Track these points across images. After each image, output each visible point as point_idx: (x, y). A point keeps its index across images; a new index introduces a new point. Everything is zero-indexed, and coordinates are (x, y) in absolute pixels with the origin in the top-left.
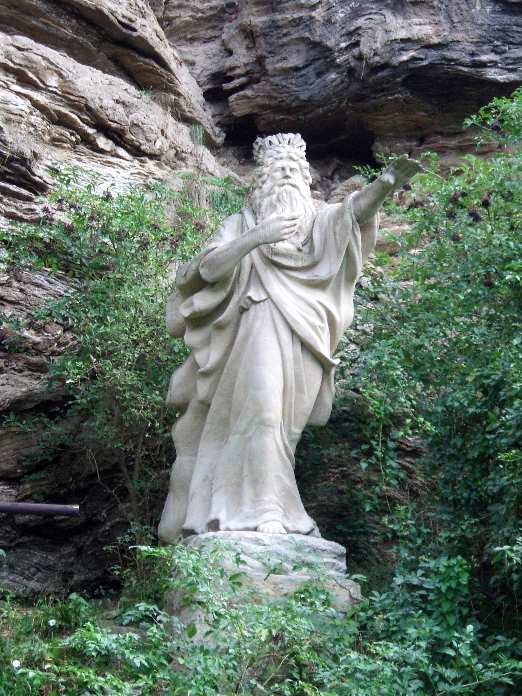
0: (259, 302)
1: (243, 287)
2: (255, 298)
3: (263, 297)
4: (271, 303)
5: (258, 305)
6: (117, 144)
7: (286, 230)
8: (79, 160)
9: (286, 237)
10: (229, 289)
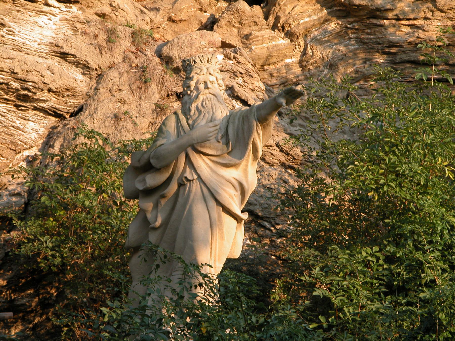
2: (190, 178)
8: (19, 11)
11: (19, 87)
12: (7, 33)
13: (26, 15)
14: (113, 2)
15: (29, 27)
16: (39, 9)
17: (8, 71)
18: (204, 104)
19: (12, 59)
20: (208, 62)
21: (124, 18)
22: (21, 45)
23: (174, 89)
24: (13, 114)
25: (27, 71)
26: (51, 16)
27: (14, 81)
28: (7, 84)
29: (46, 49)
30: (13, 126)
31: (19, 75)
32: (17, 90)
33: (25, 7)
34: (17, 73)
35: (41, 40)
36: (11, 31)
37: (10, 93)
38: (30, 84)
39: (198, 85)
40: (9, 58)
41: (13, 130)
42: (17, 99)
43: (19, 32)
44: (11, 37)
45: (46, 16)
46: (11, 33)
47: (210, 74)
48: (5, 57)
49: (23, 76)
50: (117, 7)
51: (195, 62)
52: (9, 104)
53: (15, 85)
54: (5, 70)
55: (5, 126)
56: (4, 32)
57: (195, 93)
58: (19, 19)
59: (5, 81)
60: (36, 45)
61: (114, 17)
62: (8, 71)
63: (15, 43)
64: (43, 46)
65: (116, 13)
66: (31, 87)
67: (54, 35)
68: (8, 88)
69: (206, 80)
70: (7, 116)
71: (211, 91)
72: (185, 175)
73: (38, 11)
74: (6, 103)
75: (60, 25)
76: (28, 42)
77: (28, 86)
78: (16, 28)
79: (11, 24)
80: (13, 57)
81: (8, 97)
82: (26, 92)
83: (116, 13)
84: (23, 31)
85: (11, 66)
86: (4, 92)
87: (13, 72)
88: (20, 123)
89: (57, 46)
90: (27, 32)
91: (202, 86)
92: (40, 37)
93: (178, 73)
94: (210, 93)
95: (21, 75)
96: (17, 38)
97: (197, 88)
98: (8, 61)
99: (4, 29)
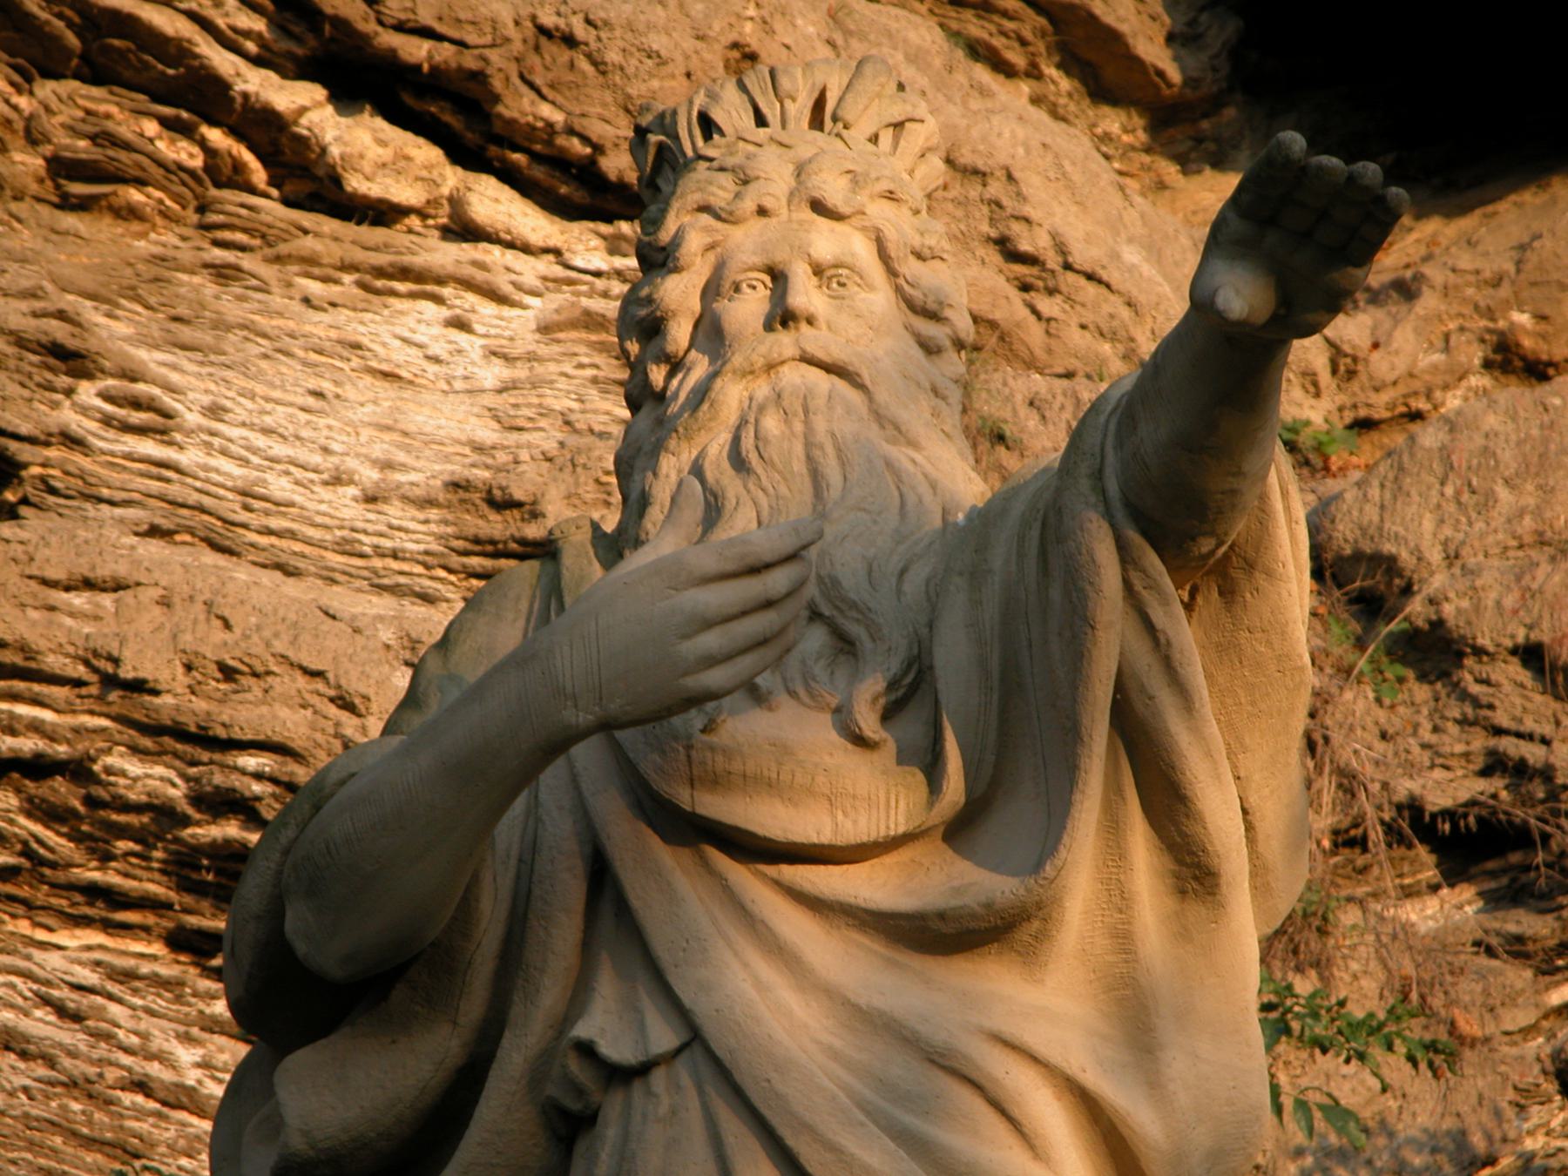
0: (643, 1070)
1: (550, 995)
2: (618, 1049)
3: (663, 1037)
4: (706, 1071)
5: (637, 1086)
6: (465, 156)
7: (711, 641)
8: (223, 274)
9: (715, 678)
10: (473, 1006)
11: (177, 793)
12: (107, 421)
13: (277, 300)
14: (1017, 228)
15: (294, 378)
16: (381, 259)
17: (81, 671)
18: (748, 442)
19: (118, 586)
20: (817, 121)
21: (1110, 336)
22: (231, 506)
23: (1405, 787)
24: (160, 1004)
25: (228, 673)
26: (471, 298)
27: (135, 750)
28: (79, 770)
29: (419, 532)
30: (141, 1086)
31: (167, 699)
32: (165, 814)
33: (283, 248)
34: (138, 686)
35: (387, 465)
36: (136, 404)
37: (123, 845)
38: (250, 761)
39: (722, 306)
40: (88, 584)
41: (141, 1114)
42: (185, 886)
43: (215, 411)
44: (148, 447)
45: (438, 300)
46: (137, 417)
47: (818, 207)
48: (53, 573)
49: (200, 705)
50: (1053, 261)
51: (708, 126)
52: (125, 927)
53: (144, 776)
54: (54, 662)
55: (72, 1084)
56: (84, 410)
57: (700, 366)
58: (221, 325)
59: (62, 750)
60: (344, 505)
61: (1034, 334)
62: (81, 671)
63: (174, 490)
64: (395, 512)
65: (1047, 305)
66: (257, 788)
67: (487, 433)
68: (91, 802)
69: (779, 256)
70: (100, 1014)
71: (811, 339)
72: (582, 1030)
73: (380, 272)
74: (108, 926)
75: (532, 357)
76: (279, 486)
77: (236, 781)
78: (188, 385)
79: (145, 356)
80: (122, 569)
81: (112, 878)
82: (230, 829)
83: (1047, 305)
84: (242, 409)
85: (99, 634)
86: (76, 837)
87: (114, 683)
88: (205, 1065)
89: (502, 503)
90: (278, 416)
91: (747, 309)
92: (378, 451)
93: (1444, 675)
94: (808, 360)
95: (176, 700)
96: (189, 457)
97: (711, 333)
98: (78, 600)
99: (87, 392)
